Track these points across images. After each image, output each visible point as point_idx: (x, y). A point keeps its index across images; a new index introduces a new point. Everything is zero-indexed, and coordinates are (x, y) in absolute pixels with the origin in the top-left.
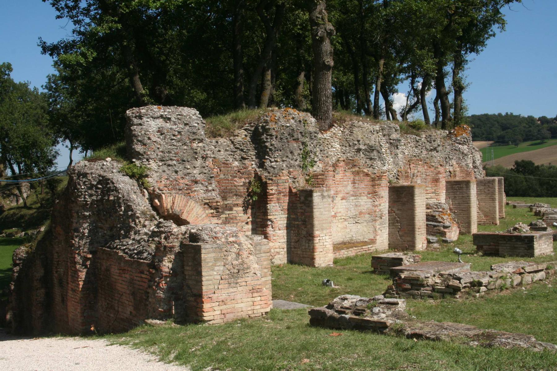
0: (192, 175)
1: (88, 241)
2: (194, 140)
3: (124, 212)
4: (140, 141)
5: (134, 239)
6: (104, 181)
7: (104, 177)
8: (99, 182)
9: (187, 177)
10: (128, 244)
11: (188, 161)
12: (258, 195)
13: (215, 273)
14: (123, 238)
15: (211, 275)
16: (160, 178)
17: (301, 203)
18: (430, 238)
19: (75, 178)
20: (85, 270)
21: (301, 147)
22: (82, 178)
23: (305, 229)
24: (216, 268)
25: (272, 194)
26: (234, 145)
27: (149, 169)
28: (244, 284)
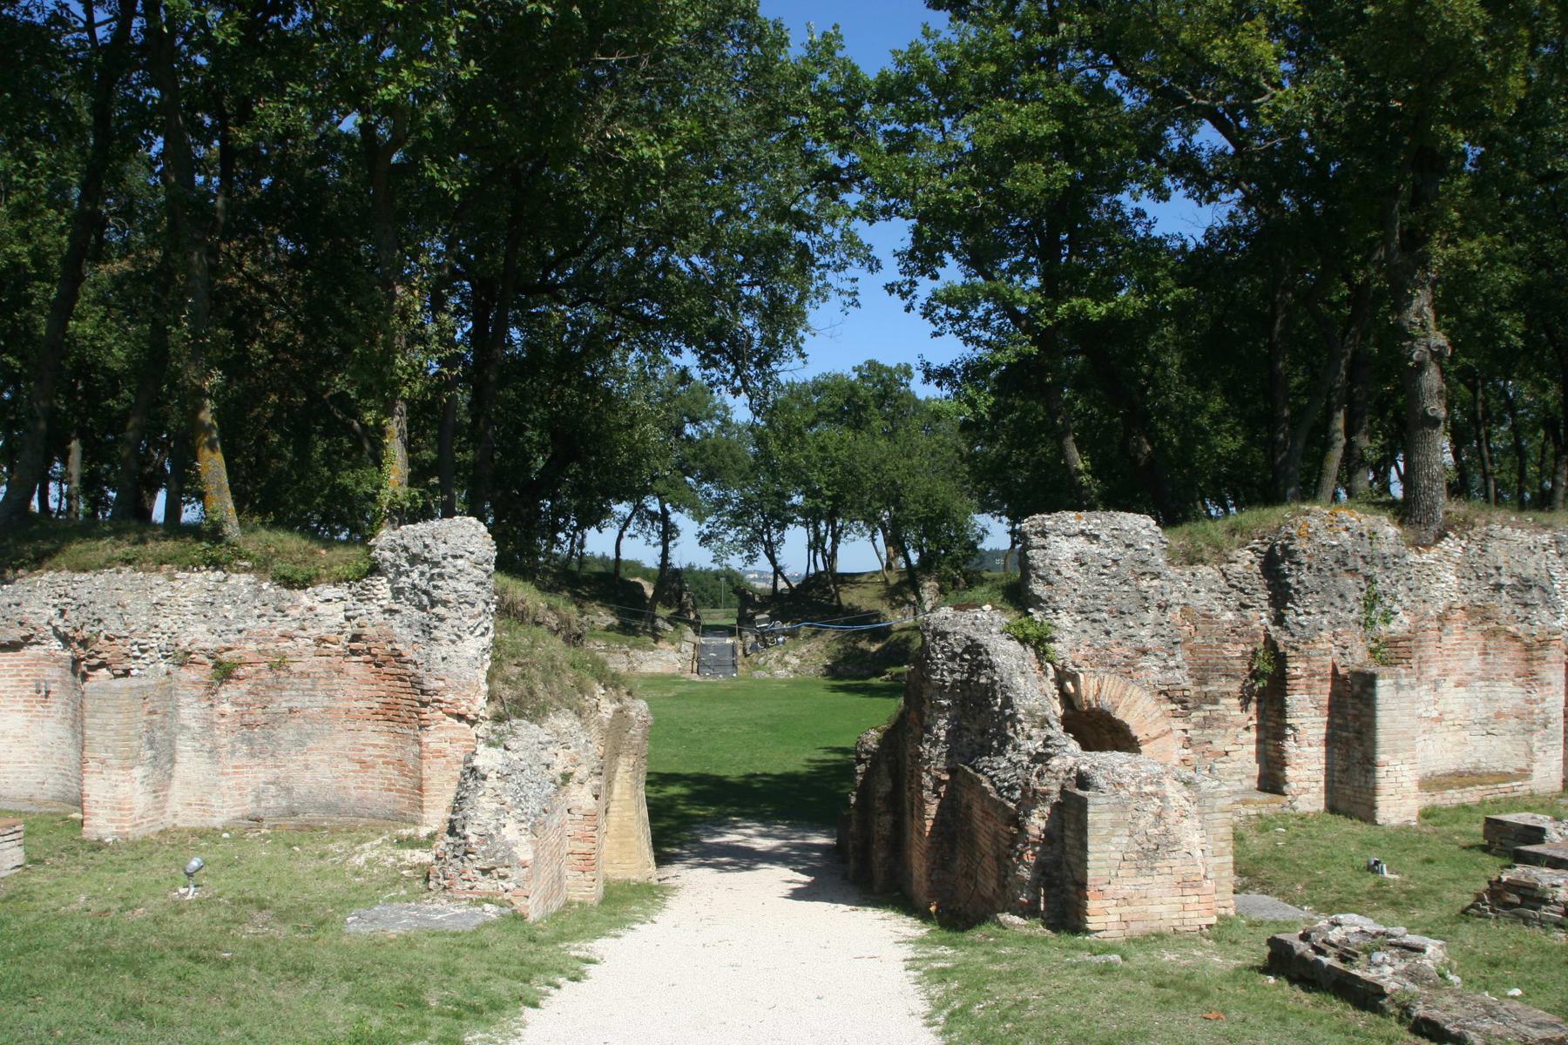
4: (1042, 578)
6: (974, 648)
8: (966, 650)
12: (1271, 678)
15: (1104, 853)
20: (937, 801)
21: (1363, 585)
24: (1115, 840)
25: (1297, 678)
28: (1167, 870)
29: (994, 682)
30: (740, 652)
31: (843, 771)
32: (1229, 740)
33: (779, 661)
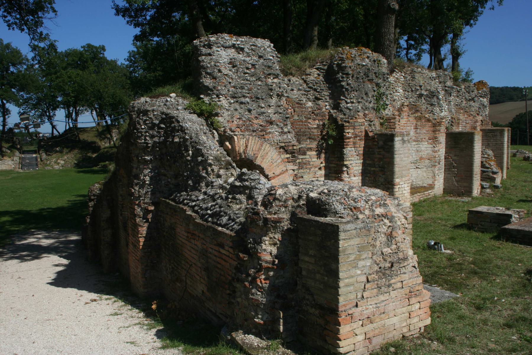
0: (267, 114)
1: (150, 190)
2: (270, 74)
3: (192, 157)
4: (209, 74)
5: (205, 193)
7: (168, 114)
8: (162, 121)
9: (261, 117)
10: (198, 200)
11: (263, 99)
13: (359, 272)
14: (192, 191)
16: (232, 118)
17: (379, 148)
18: (484, 183)
19: (134, 116)
20: (146, 225)
22: (143, 116)
23: (383, 176)
24: (361, 263)
26: (307, 84)
27: (221, 107)
28: (399, 285)
29: (186, 140)
30: (39, 160)
31: (84, 205)
32: (311, 175)
33: (55, 162)
